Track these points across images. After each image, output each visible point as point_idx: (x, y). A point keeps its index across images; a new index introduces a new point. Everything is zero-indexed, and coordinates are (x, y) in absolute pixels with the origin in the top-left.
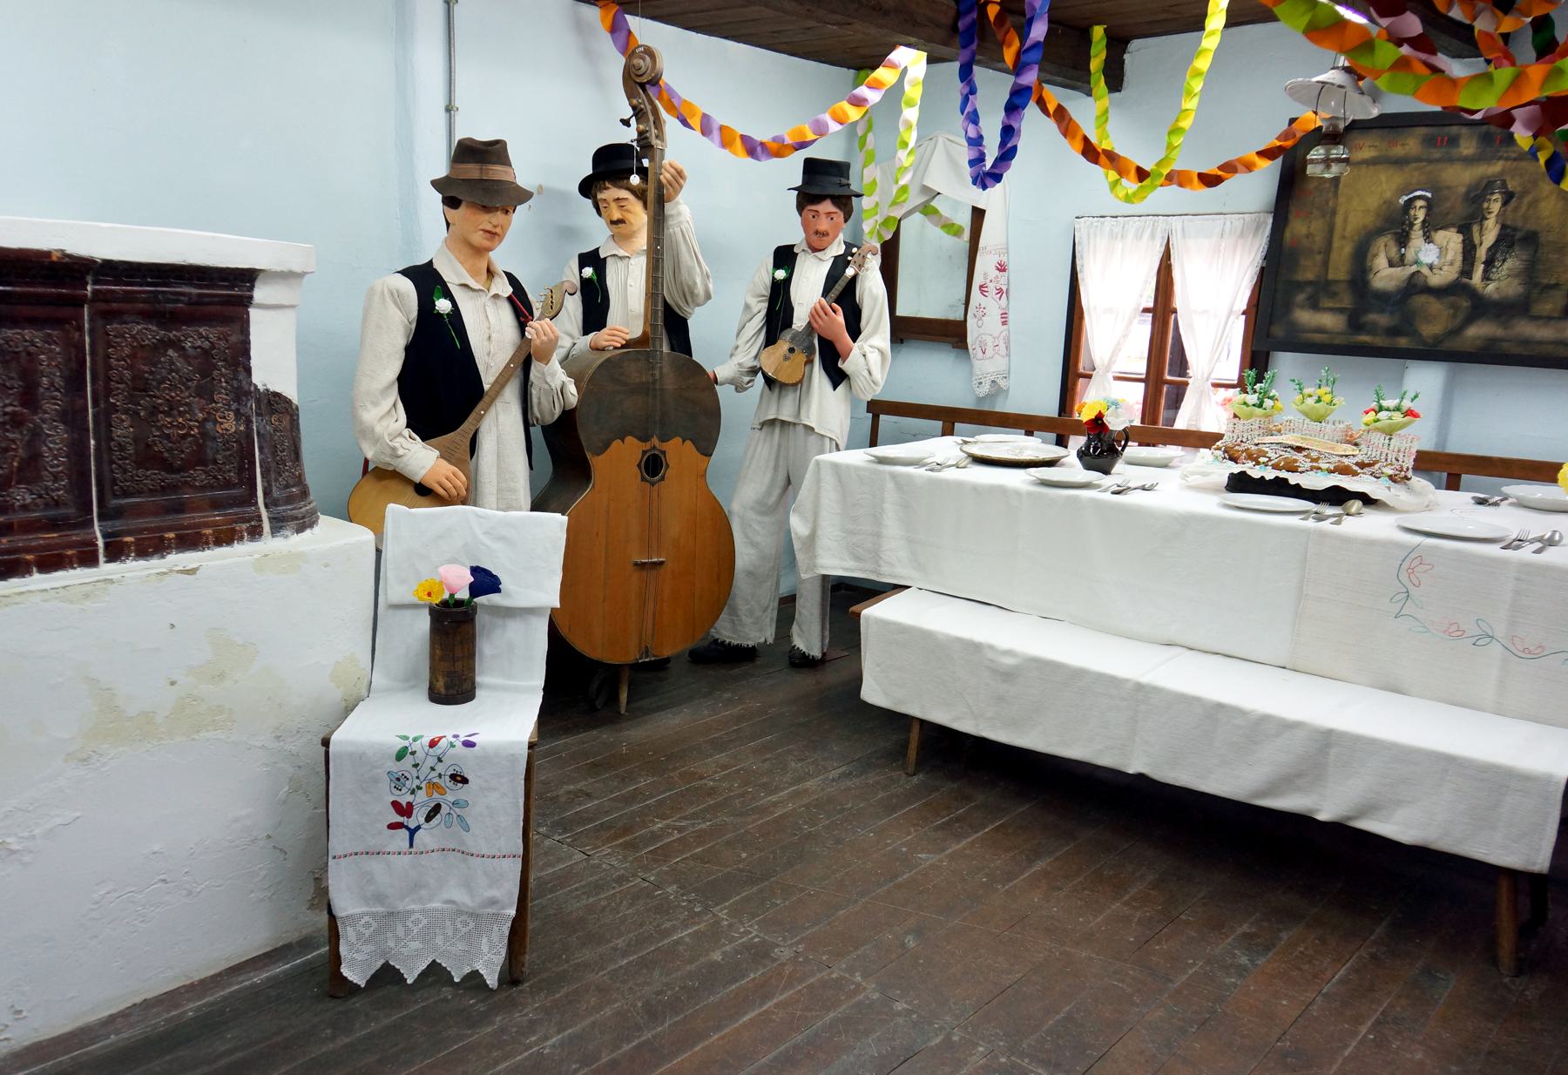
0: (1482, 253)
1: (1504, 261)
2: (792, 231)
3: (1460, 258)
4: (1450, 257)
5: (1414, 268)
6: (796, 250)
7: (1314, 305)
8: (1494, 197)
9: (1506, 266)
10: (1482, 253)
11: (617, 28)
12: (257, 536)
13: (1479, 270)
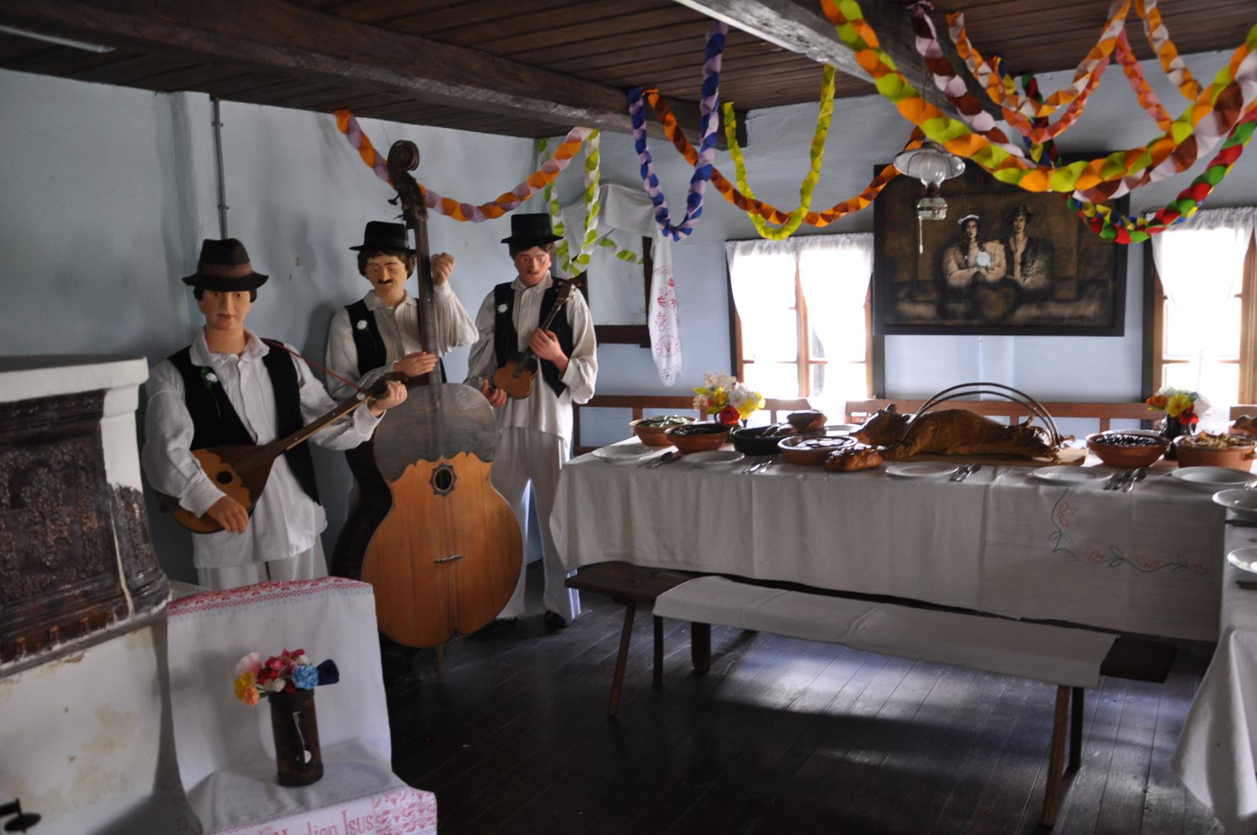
0: (1018, 257)
1: (1033, 262)
2: (509, 273)
3: (1004, 261)
4: (997, 260)
5: (975, 270)
6: (513, 287)
7: (912, 299)
8: (1020, 218)
9: (1034, 266)
10: (1018, 257)
11: (349, 130)
12: (124, 615)
13: (1018, 268)
